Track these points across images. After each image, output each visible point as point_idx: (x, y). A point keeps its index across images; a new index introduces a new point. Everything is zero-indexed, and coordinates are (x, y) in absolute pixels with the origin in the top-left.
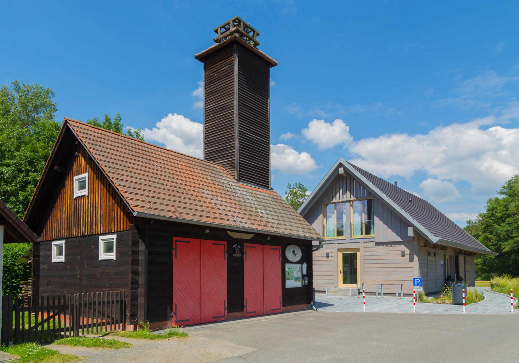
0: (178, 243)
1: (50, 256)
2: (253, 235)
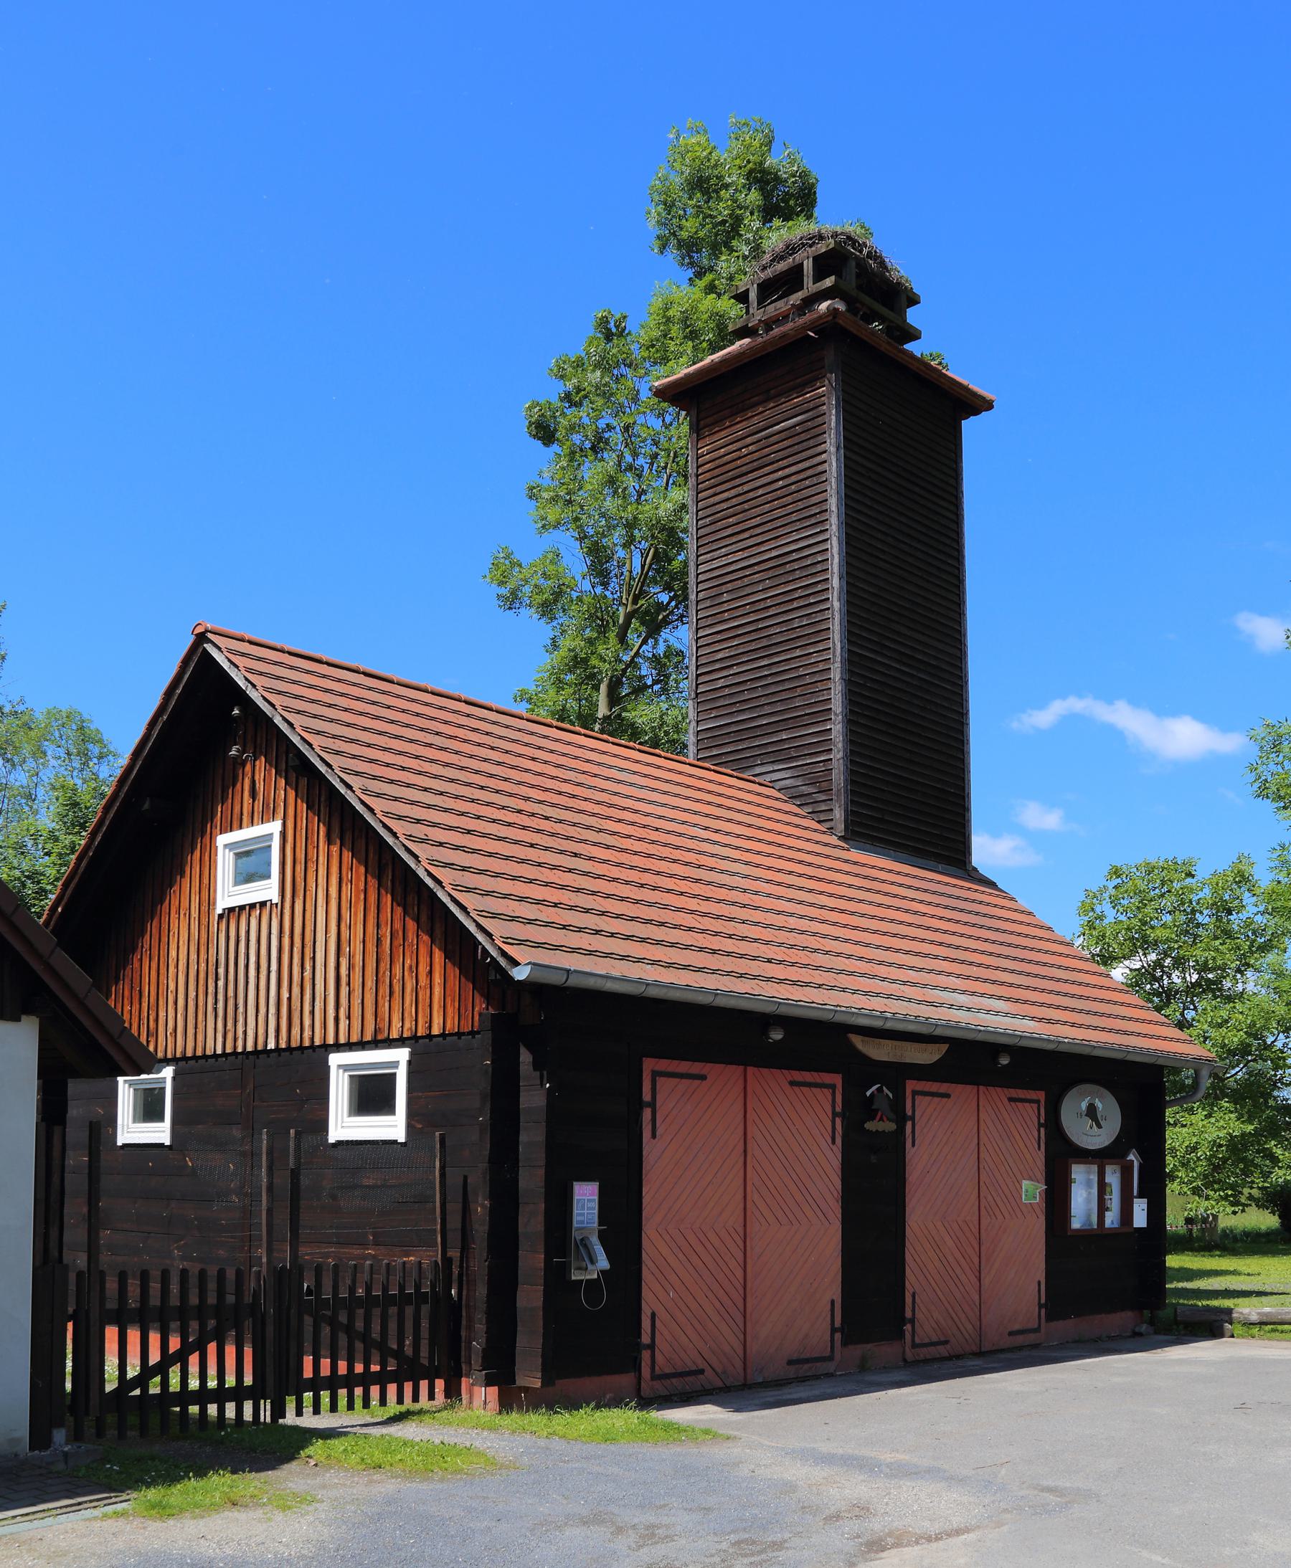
0: (661, 1081)
1: (322, 1125)
2: (945, 1047)
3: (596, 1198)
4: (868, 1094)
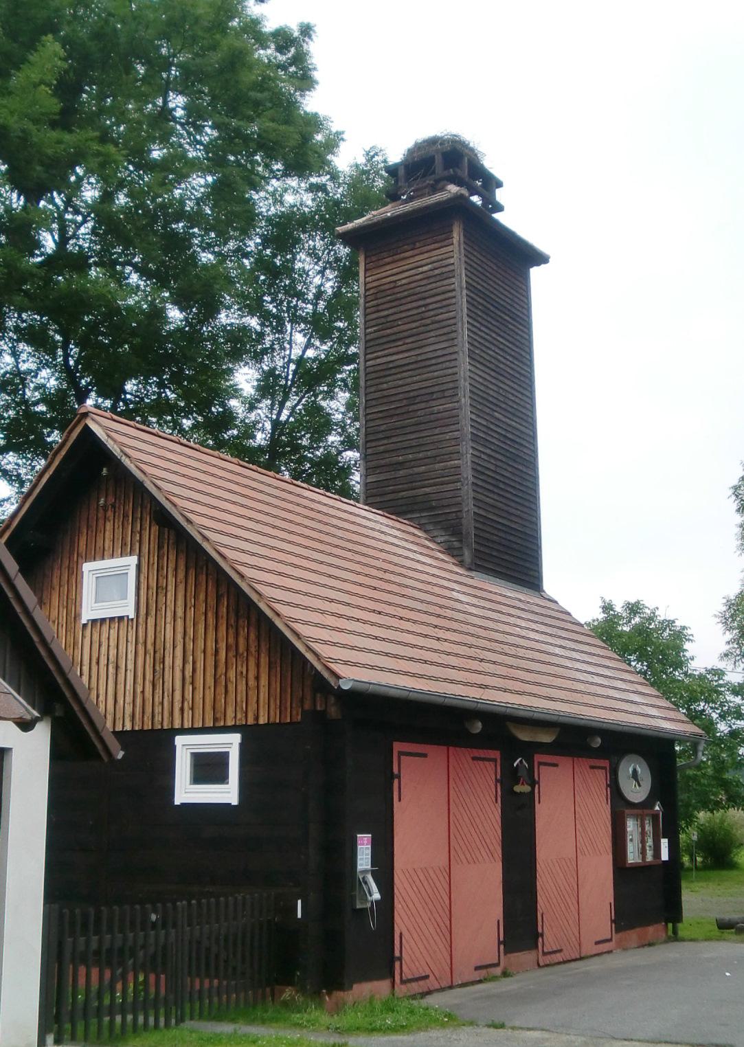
1: (168, 789)
3: (370, 846)
4: (515, 765)
